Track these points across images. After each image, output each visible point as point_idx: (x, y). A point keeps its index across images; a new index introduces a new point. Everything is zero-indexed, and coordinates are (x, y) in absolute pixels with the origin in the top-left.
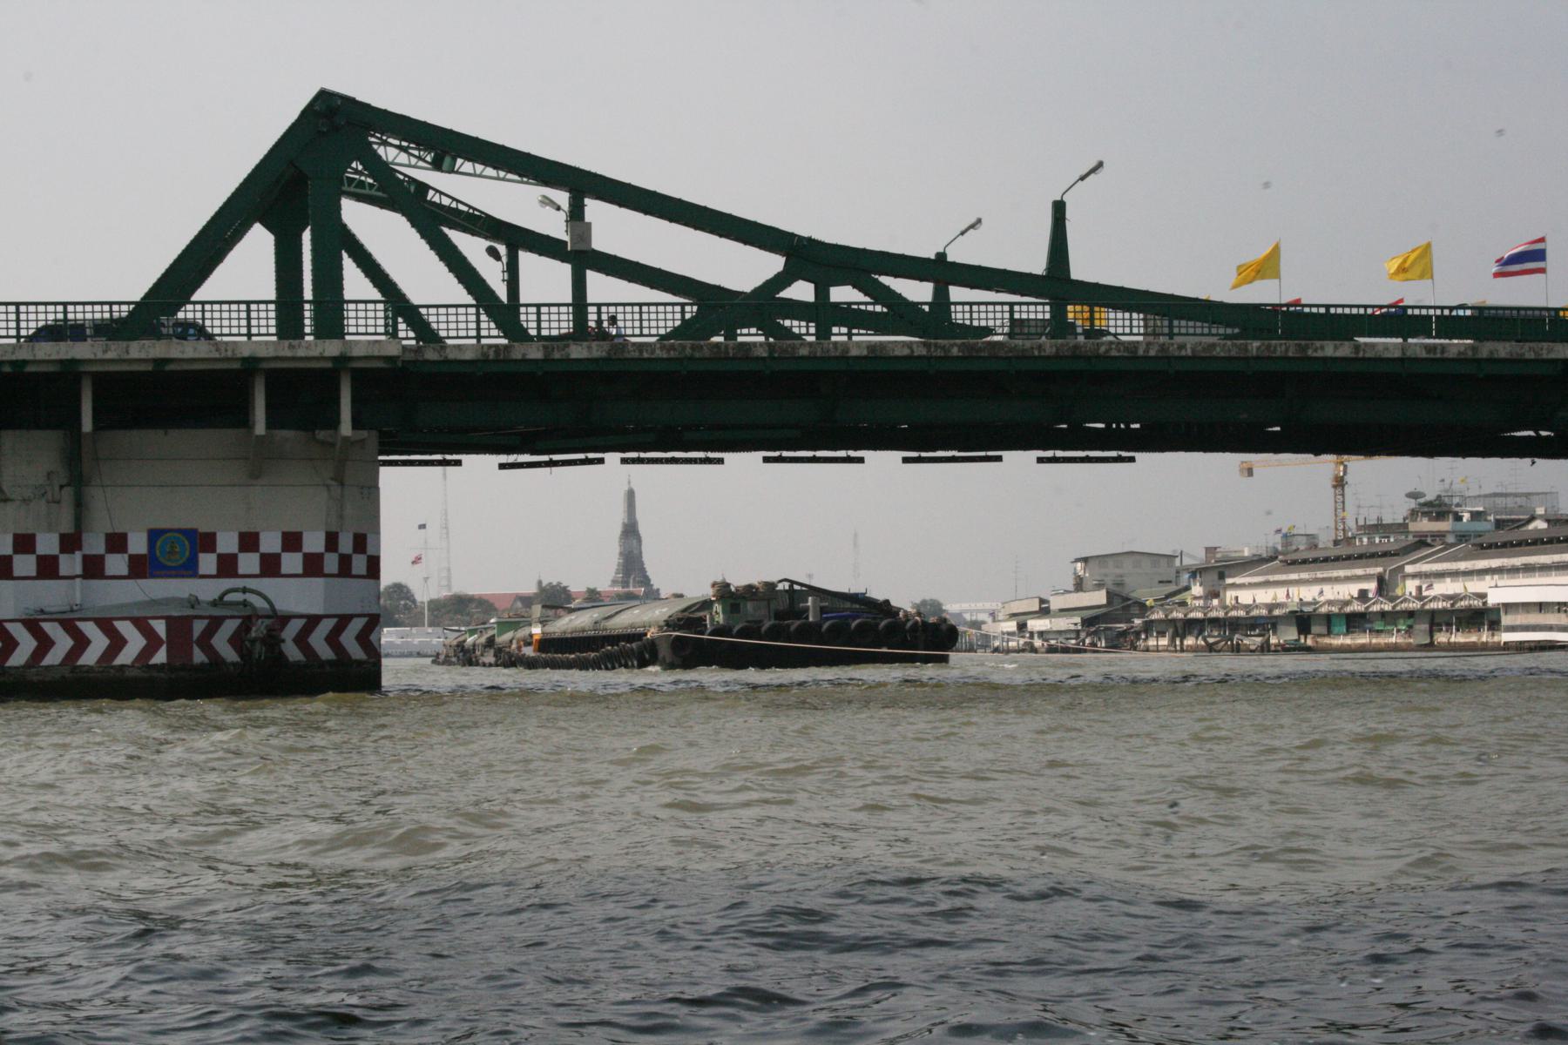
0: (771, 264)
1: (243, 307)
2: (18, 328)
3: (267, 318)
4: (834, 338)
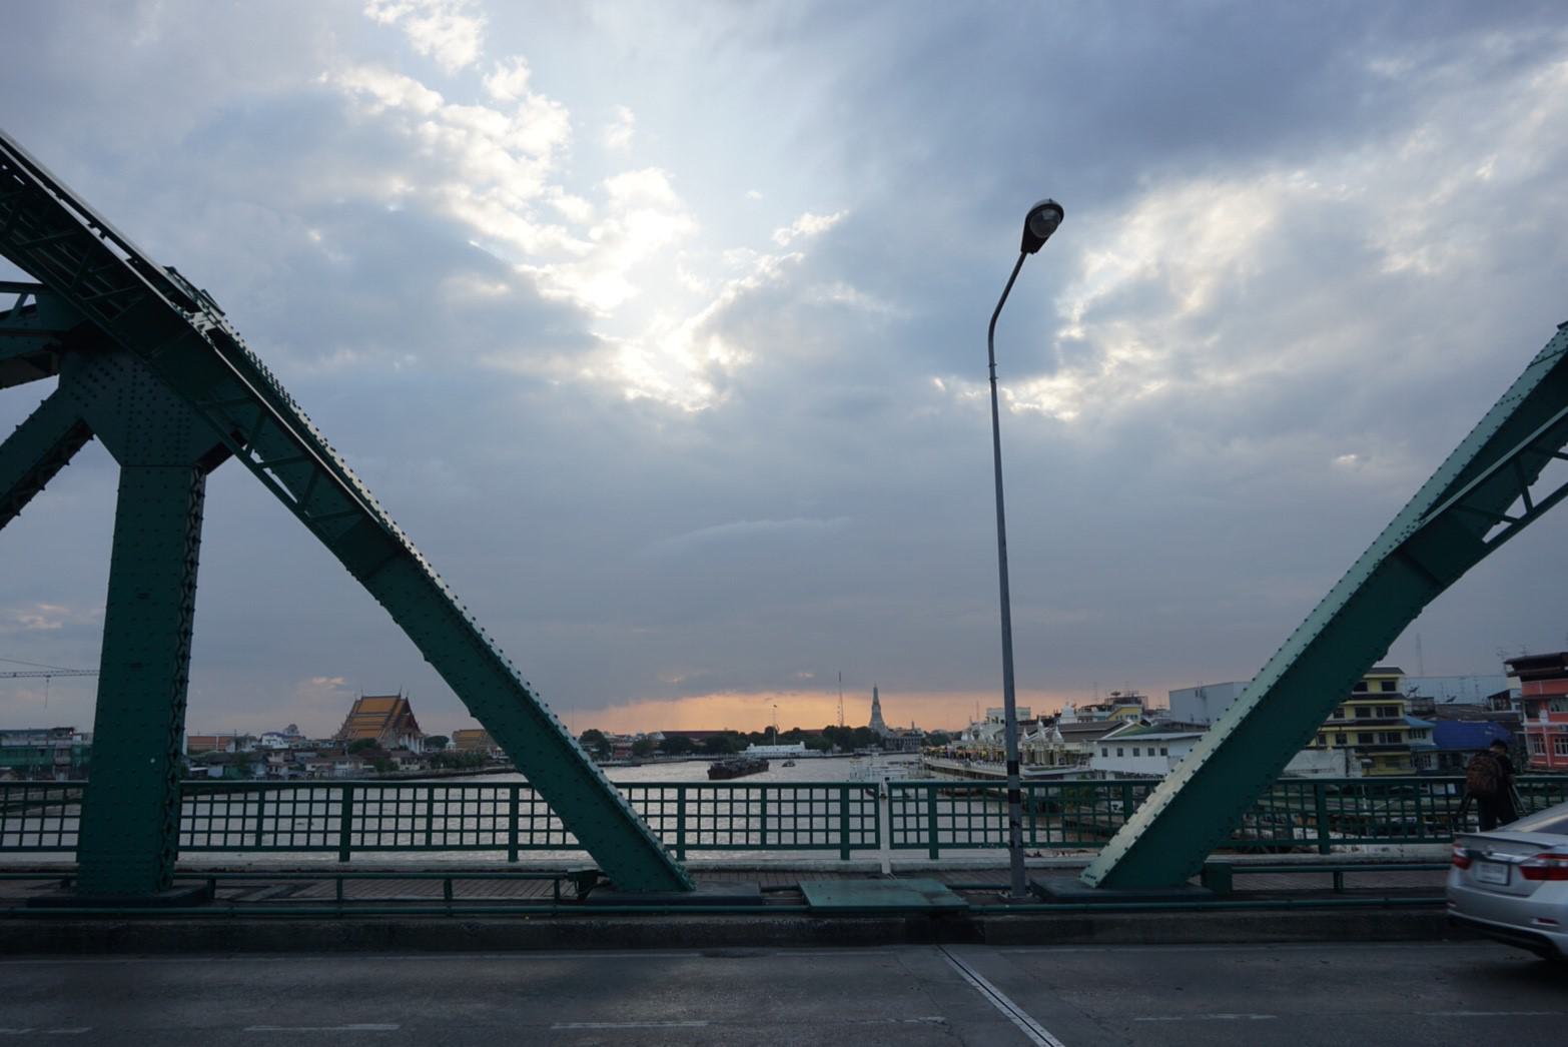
0: (15, 297)
1: (835, 794)
4: (185, 858)
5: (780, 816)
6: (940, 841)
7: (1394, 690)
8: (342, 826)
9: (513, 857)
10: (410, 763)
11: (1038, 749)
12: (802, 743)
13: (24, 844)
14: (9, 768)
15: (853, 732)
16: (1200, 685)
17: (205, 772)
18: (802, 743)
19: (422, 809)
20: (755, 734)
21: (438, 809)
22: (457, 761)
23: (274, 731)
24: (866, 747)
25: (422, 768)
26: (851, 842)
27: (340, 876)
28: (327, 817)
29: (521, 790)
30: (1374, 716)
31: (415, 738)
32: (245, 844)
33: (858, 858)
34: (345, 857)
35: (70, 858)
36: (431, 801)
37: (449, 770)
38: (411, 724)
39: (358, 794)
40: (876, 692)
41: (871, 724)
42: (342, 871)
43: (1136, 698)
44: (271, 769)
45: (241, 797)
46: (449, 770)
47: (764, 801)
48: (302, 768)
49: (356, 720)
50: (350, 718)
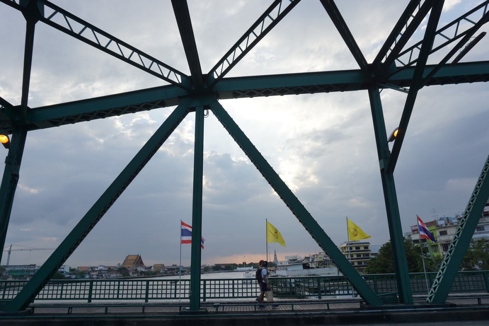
2: (148, 285)
5: (238, 288)
7: (368, 249)
10: (134, 274)
12: (252, 267)
13: (123, 297)
14: (11, 276)
17: (71, 277)
18: (252, 267)
19: (116, 287)
20: (240, 264)
21: (121, 287)
23: (102, 265)
25: (138, 275)
27: (143, 306)
28: (153, 289)
29: (207, 281)
30: (362, 257)
31: (142, 267)
34: (147, 301)
35: (188, 300)
36: (119, 285)
38: (141, 263)
39: (94, 283)
41: (274, 261)
44: (91, 276)
45: (70, 284)
47: (233, 284)
49: (126, 262)
50: (125, 261)
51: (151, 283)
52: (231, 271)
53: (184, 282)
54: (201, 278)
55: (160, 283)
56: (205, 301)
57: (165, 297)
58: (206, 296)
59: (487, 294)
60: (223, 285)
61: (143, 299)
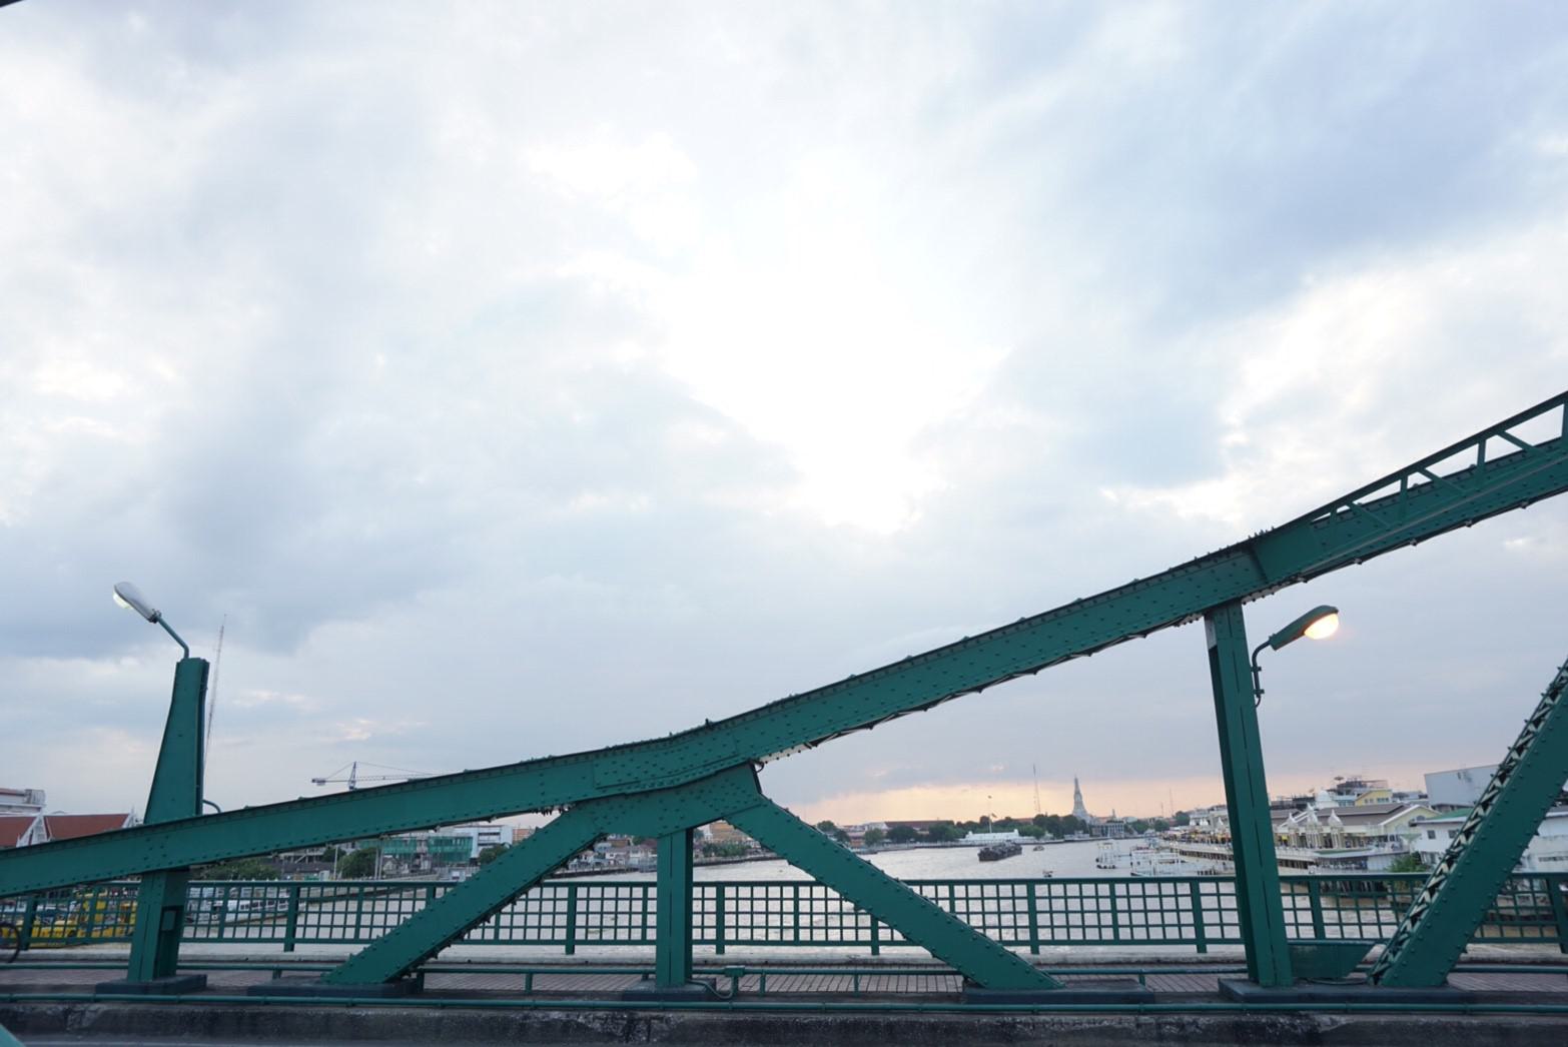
1: (1021, 890)
2: (572, 900)
3: (1178, 911)
6: (1207, 936)
8: (691, 918)
9: (875, 952)
11: (1309, 832)
12: (1016, 831)
15: (1061, 820)
16: (1463, 767)
18: (1016, 831)
22: (726, 851)
24: (1073, 834)
26: (727, 938)
32: (770, 938)
33: (582, 952)
35: (649, 951)
37: (721, 859)
40: (1076, 781)
42: (746, 964)
43: (1360, 782)
46: (721, 859)
48: (603, 857)
51: (582, 892)
52: (949, 843)
53: (734, 888)
54: (695, 879)
55: (610, 892)
56: (1205, 951)
57: (535, 937)
58: (880, 939)
59: (1554, 951)
60: (980, 901)
61: (559, 942)
